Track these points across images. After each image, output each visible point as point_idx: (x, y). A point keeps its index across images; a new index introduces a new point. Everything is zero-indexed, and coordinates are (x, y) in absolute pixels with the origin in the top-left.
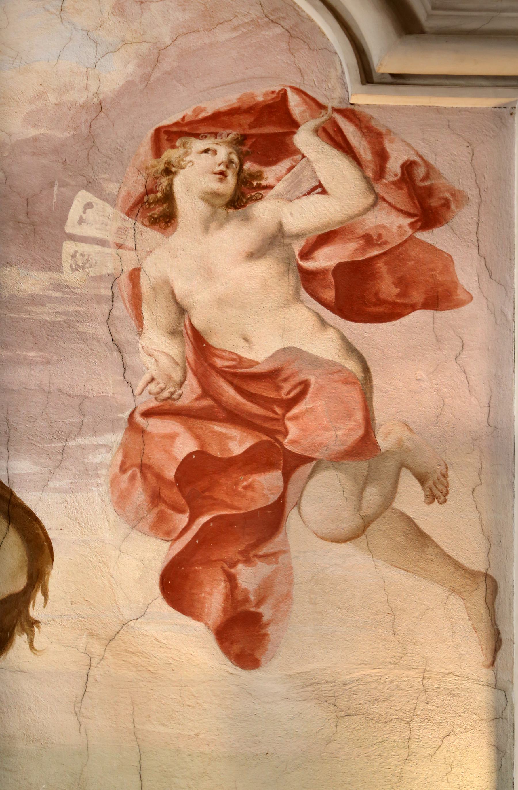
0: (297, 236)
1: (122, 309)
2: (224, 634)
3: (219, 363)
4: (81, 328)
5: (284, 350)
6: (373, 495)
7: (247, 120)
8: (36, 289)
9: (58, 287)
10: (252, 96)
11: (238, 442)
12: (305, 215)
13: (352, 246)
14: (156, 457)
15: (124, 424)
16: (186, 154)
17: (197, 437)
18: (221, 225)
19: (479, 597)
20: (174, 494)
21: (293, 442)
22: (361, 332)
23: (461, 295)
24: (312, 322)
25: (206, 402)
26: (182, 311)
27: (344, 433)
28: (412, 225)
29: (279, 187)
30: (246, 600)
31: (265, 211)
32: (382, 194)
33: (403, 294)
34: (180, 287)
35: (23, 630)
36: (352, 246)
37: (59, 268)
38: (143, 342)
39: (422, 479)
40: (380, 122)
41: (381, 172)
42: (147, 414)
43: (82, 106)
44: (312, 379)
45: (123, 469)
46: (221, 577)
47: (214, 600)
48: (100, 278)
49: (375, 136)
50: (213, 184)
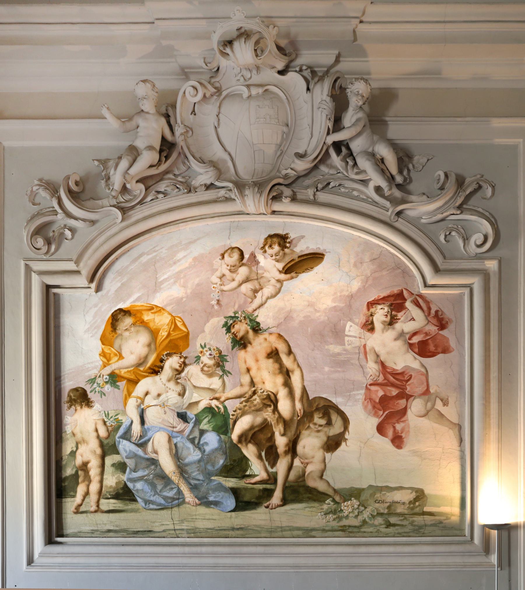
0: (407, 333)
1: (362, 356)
2: (393, 441)
3: (388, 370)
4: (352, 362)
5: (405, 366)
6: (429, 405)
7: (392, 299)
8: (339, 351)
9: (345, 350)
10: (393, 291)
11: (394, 392)
12: (409, 327)
13: (422, 336)
14: (374, 396)
15: (365, 388)
16: (376, 310)
17: (384, 391)
18: (387, 331)
19: (456, 430)
20: (378, 406)
21: (408, 391)
22: (425, 361)
23: (451, 349)
24: (413, 358)
25: (386, 381)
26: (378, 356)
28: (438, 329)
29: (402, 319)
30: (398, 432)
31: (398, 326)
32: (430, 320)
33: (436, 350)
34: (377, 349)
35: (344, 441)
36: (422, 336)
37: (344, 345)
38: (368, 365)
39: (442, 400)
40: (429, 298)
41: (429, 314)
42: (370, 385)
43: (347, 296)
44: (413, 374)
45: (365, 400)
46: (392, 427)
48: (356, 347)
49: (427, 302)
50: (384, 318)
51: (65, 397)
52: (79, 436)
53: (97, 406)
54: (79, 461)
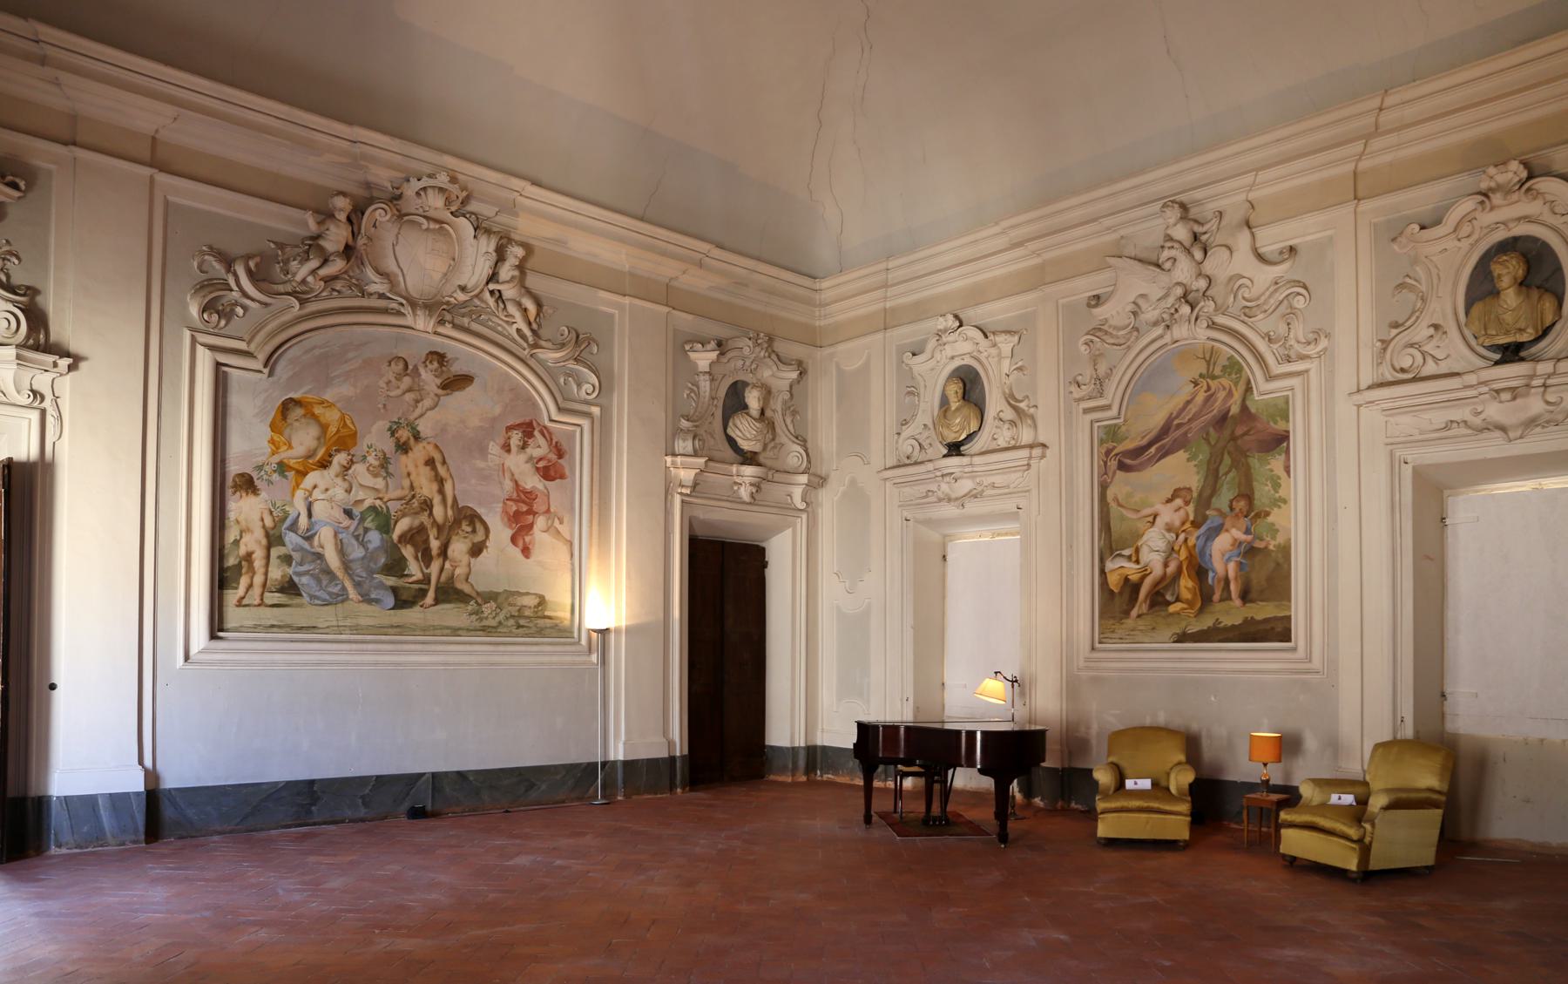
11: (525, 508)
12: (537, 453)
27: (544, 508)
31: (529, 450)
47: (521, 543)
51: (229, 482)
52: (243, 523)
53: (263, 495)
54: (243, 550)
